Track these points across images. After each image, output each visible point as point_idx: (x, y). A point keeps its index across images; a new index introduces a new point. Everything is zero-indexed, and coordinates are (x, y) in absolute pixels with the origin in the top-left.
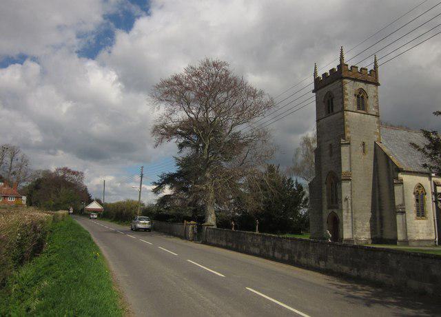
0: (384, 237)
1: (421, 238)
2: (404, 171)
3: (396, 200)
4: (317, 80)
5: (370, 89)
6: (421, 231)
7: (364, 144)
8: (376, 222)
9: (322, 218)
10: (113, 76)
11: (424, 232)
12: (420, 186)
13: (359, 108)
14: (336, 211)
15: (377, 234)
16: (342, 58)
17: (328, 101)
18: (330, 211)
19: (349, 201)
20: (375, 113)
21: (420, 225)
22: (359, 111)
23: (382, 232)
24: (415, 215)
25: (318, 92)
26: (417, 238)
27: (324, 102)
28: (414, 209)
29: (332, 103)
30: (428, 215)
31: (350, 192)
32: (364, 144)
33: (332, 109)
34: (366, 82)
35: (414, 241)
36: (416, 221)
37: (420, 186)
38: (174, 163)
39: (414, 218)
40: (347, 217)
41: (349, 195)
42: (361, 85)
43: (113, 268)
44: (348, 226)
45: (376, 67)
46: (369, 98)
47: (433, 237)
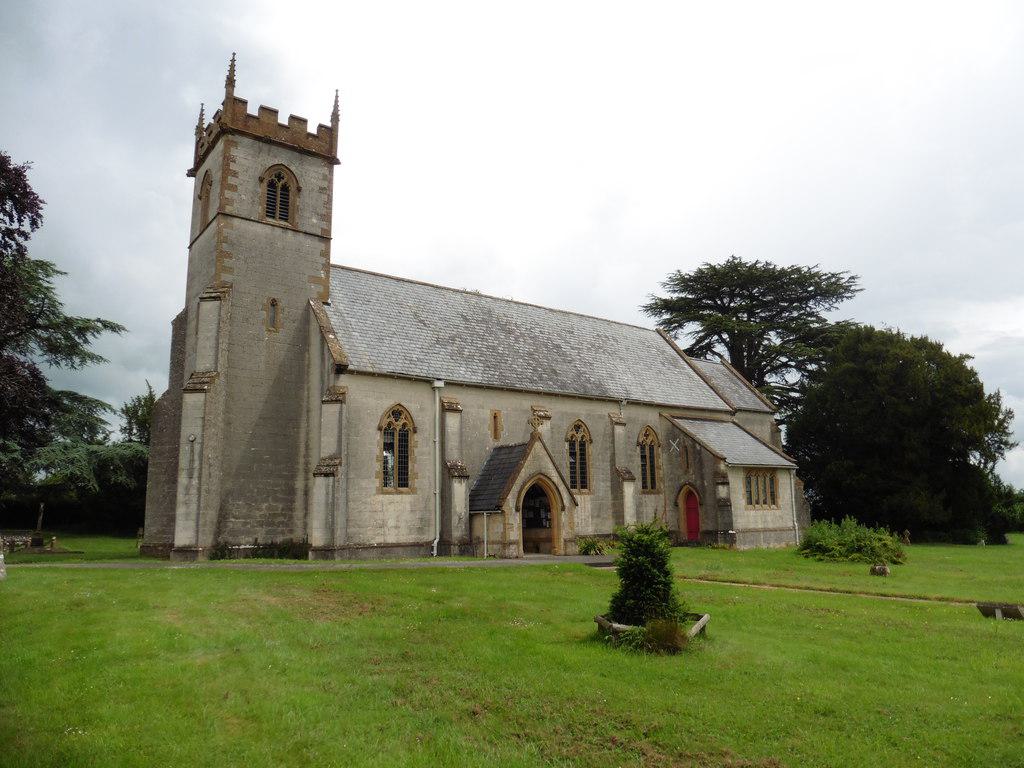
1: (391, 539)
2: (352, 372)
6: (391, 523)
11: (403, 524)
13: (270, 213)
15: (291, 531)
16: (230, 82)
19: (197, 447)
21: (391, 508)
22: (270, 220)
23: (305, 525)
24: (377, 483)
26: (379, 540)
30: (780, 501)
31: (200, 422)
32: (274, 303)
36: (381, 497)
37: (397, 412)
40: (187, 489)
41: (198, 431)
42: (282, 158)
44: (187, 515)
46: (305, 192)
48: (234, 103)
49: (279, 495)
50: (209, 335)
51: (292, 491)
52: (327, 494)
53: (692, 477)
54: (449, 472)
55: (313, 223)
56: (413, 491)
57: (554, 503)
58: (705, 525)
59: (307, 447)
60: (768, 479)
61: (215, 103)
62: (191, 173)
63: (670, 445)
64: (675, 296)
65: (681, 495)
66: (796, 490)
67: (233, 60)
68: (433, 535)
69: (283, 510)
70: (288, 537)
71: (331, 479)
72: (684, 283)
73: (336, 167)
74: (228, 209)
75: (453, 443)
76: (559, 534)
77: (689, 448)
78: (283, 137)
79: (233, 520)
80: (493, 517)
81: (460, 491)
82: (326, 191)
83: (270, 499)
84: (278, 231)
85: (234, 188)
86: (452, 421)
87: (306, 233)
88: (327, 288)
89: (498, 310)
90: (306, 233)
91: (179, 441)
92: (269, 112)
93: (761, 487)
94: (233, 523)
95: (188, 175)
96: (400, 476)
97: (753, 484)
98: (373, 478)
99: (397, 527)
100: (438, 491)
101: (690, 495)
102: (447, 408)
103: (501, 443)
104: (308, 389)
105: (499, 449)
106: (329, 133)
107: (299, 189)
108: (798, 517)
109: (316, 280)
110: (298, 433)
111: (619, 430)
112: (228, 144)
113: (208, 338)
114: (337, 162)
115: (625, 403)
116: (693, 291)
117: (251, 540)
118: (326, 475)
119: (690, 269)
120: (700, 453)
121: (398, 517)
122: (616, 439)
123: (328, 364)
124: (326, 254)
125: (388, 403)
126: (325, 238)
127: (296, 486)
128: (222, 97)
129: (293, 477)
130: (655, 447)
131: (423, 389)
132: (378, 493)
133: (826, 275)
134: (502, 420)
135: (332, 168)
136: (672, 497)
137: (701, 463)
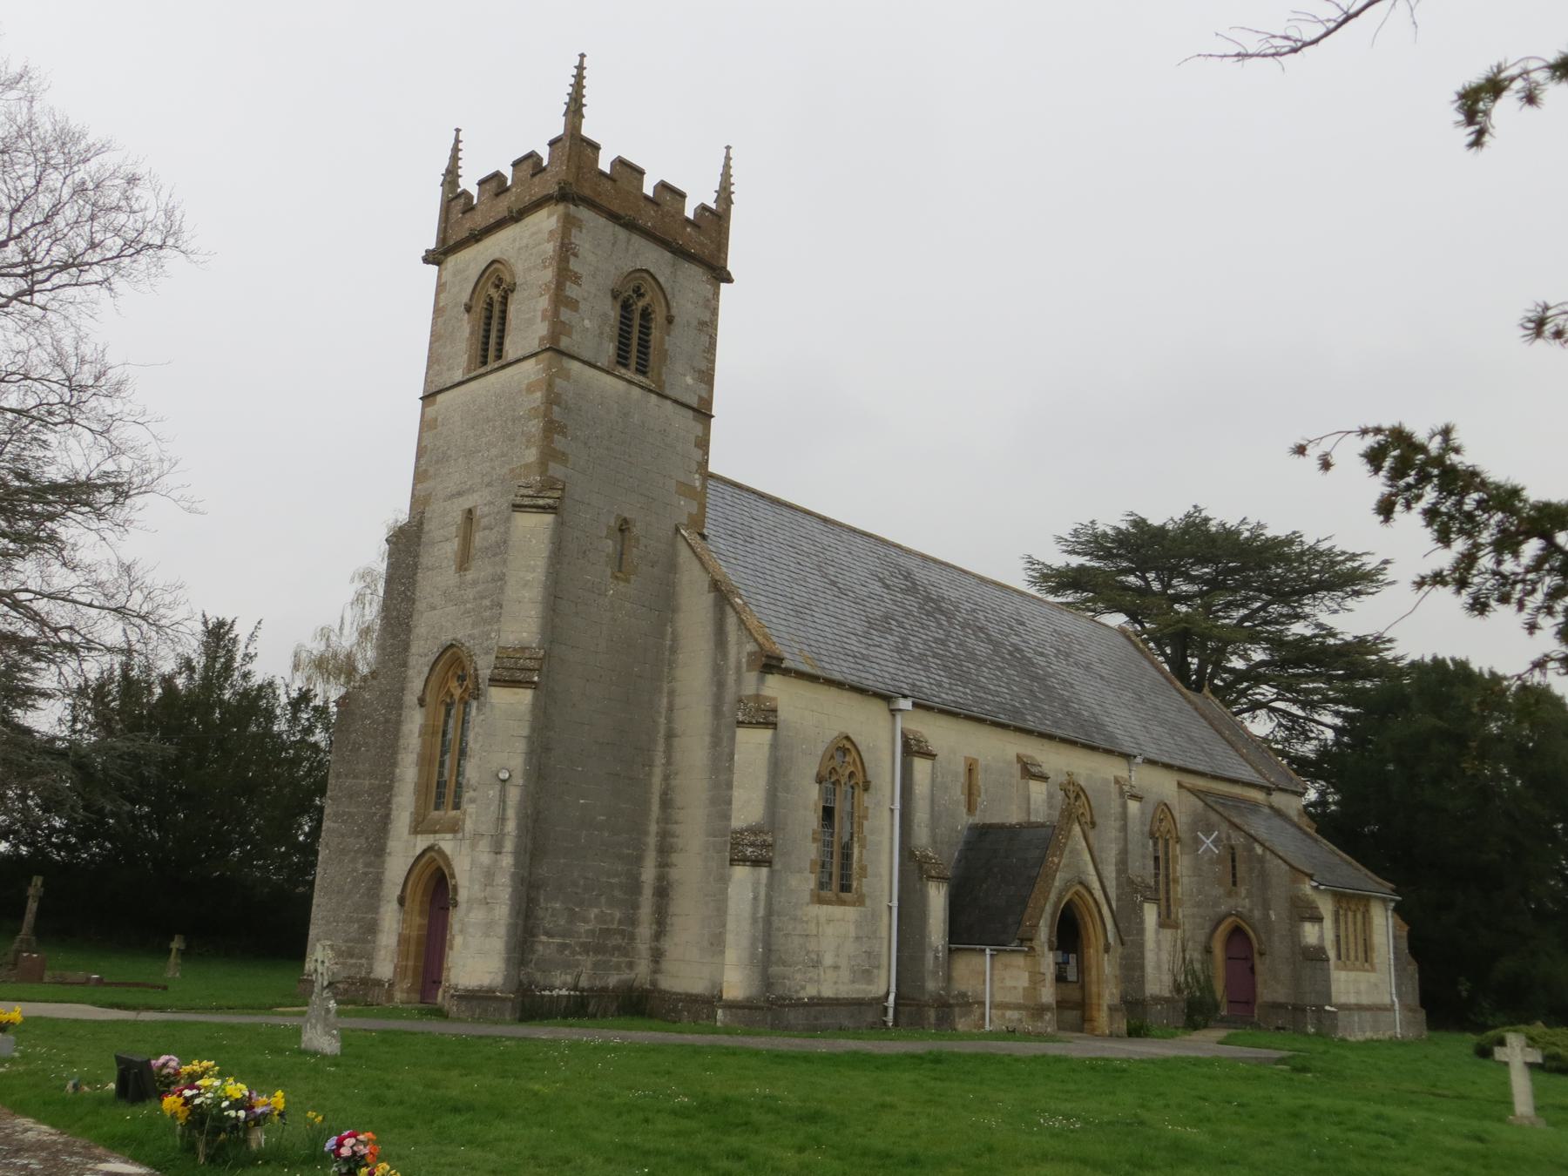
0: (666, 983)
1: (828, 992)
3: (735, 805)
4: (454, 200)
5: (686, 282)
6: (828, 960)
7: (624, 527)
8: (636, 907)
9: (378, 881)
10: (1540, 1023)
11: (843, 963)
12: (845, 747)
13: (622, 358)
14: (447, 844)
15: (631, 965)
16: (575, 108)
17: (490, 304)
18: (422, 842)
20: (694, 402)
21: (829, 930)
23: (657, 956)
25: (452, 261)
26: (811, 991)
27: (468, 309)
28: (812, 851)
29: (504, 312)
32: (624, 527)
33: (500, 344)
34: (681, 253)
35: (798, 1004)
37: (845, 747)
38: (268, 678)
39: (807, 897)
42: (652, 258)
43: (797, 1041)
45: (725, 194)
47: (877, 989)
48: (575, 144)
49: (617, 893)
50: (530, 577)
51: (635, 887)
52: (755, 898)
53: (1243, 903)
54: (914, 867)
55: (684, 383)
56: (860, 901)
57: (1093, 939)
58: (1272, 988)
59: (666, 803)
60: (1359, 916)
61: (538, 132)
62: (432, 258)
63: (1197, 842)
64: (1076, 561)
65: (1222, 928)
66: (1395, 937)
67: (580, 68)
68: (884, 984)
69: (620, 922)
70: (626, 975)
71: (764, 871)
72: (1097, 544)
73: (723, 285)
74: (564, 343)
75: (921, 815)
76: (1099, 996)
77: (1239, 852)
78: (648, 219)
79: (544, 938)
80: (1004, 959)
81: (937, 898)
82: (708, 326)
83: (603, 899)
84: (636, 392)
85: (573, 305)
86: (921, 766)
87: (676, 401)
88: (703, 507)
89: (920, 575)
90: (676, 401)
91: (393, 773)
92: (628, 171)
93: (1351, 929)
94: (545, 946)
95: (426, 260)
96: (839, 877)
97: (1342, 919)
98: (807, 874)
99: (836, 967)
100: (895, 903)
101: (1237, 933)
102: (913, 749)
103: (977, 819)
104: (672, 693)
105: (973, 828)
106: (716, 220)
107: (670, 320)
108: (1398, 986)
109: (686, 490)
110: (650, 775)
111: (1133, 806)
112: (569, 223)
113: (526, 584)
114: (728, 279)
115: (1139, 760)
116: (1109, 555)
117: (569, 979)
118: (756, 863)
119: (1112, 519)
120: (1261, 860)
121: (839, 947)
122: (1130, 824)
123: (739, 649)
124: (703, 444)
125: (832, 732)
126: (703, 413)
127: (644, 878)
128: (558, 128)
129: (638, 860)
130: (1171, 842)
131: (878, 709)
132: (812, 902)
133: (1343, 553)
134: (980, 778)
135: (719, 287)
136: (1201, 936)
137: (1264, 877)
